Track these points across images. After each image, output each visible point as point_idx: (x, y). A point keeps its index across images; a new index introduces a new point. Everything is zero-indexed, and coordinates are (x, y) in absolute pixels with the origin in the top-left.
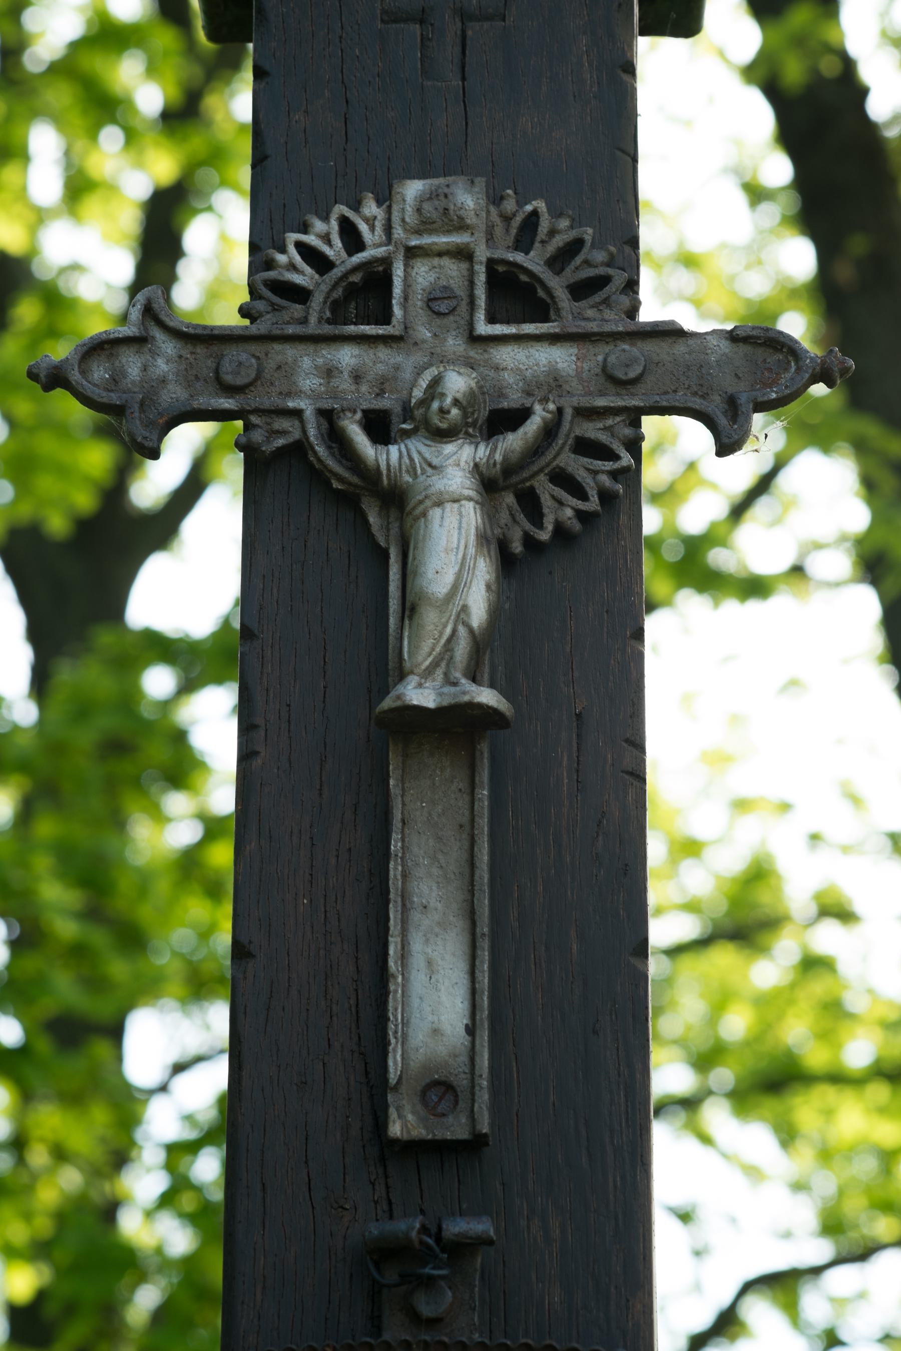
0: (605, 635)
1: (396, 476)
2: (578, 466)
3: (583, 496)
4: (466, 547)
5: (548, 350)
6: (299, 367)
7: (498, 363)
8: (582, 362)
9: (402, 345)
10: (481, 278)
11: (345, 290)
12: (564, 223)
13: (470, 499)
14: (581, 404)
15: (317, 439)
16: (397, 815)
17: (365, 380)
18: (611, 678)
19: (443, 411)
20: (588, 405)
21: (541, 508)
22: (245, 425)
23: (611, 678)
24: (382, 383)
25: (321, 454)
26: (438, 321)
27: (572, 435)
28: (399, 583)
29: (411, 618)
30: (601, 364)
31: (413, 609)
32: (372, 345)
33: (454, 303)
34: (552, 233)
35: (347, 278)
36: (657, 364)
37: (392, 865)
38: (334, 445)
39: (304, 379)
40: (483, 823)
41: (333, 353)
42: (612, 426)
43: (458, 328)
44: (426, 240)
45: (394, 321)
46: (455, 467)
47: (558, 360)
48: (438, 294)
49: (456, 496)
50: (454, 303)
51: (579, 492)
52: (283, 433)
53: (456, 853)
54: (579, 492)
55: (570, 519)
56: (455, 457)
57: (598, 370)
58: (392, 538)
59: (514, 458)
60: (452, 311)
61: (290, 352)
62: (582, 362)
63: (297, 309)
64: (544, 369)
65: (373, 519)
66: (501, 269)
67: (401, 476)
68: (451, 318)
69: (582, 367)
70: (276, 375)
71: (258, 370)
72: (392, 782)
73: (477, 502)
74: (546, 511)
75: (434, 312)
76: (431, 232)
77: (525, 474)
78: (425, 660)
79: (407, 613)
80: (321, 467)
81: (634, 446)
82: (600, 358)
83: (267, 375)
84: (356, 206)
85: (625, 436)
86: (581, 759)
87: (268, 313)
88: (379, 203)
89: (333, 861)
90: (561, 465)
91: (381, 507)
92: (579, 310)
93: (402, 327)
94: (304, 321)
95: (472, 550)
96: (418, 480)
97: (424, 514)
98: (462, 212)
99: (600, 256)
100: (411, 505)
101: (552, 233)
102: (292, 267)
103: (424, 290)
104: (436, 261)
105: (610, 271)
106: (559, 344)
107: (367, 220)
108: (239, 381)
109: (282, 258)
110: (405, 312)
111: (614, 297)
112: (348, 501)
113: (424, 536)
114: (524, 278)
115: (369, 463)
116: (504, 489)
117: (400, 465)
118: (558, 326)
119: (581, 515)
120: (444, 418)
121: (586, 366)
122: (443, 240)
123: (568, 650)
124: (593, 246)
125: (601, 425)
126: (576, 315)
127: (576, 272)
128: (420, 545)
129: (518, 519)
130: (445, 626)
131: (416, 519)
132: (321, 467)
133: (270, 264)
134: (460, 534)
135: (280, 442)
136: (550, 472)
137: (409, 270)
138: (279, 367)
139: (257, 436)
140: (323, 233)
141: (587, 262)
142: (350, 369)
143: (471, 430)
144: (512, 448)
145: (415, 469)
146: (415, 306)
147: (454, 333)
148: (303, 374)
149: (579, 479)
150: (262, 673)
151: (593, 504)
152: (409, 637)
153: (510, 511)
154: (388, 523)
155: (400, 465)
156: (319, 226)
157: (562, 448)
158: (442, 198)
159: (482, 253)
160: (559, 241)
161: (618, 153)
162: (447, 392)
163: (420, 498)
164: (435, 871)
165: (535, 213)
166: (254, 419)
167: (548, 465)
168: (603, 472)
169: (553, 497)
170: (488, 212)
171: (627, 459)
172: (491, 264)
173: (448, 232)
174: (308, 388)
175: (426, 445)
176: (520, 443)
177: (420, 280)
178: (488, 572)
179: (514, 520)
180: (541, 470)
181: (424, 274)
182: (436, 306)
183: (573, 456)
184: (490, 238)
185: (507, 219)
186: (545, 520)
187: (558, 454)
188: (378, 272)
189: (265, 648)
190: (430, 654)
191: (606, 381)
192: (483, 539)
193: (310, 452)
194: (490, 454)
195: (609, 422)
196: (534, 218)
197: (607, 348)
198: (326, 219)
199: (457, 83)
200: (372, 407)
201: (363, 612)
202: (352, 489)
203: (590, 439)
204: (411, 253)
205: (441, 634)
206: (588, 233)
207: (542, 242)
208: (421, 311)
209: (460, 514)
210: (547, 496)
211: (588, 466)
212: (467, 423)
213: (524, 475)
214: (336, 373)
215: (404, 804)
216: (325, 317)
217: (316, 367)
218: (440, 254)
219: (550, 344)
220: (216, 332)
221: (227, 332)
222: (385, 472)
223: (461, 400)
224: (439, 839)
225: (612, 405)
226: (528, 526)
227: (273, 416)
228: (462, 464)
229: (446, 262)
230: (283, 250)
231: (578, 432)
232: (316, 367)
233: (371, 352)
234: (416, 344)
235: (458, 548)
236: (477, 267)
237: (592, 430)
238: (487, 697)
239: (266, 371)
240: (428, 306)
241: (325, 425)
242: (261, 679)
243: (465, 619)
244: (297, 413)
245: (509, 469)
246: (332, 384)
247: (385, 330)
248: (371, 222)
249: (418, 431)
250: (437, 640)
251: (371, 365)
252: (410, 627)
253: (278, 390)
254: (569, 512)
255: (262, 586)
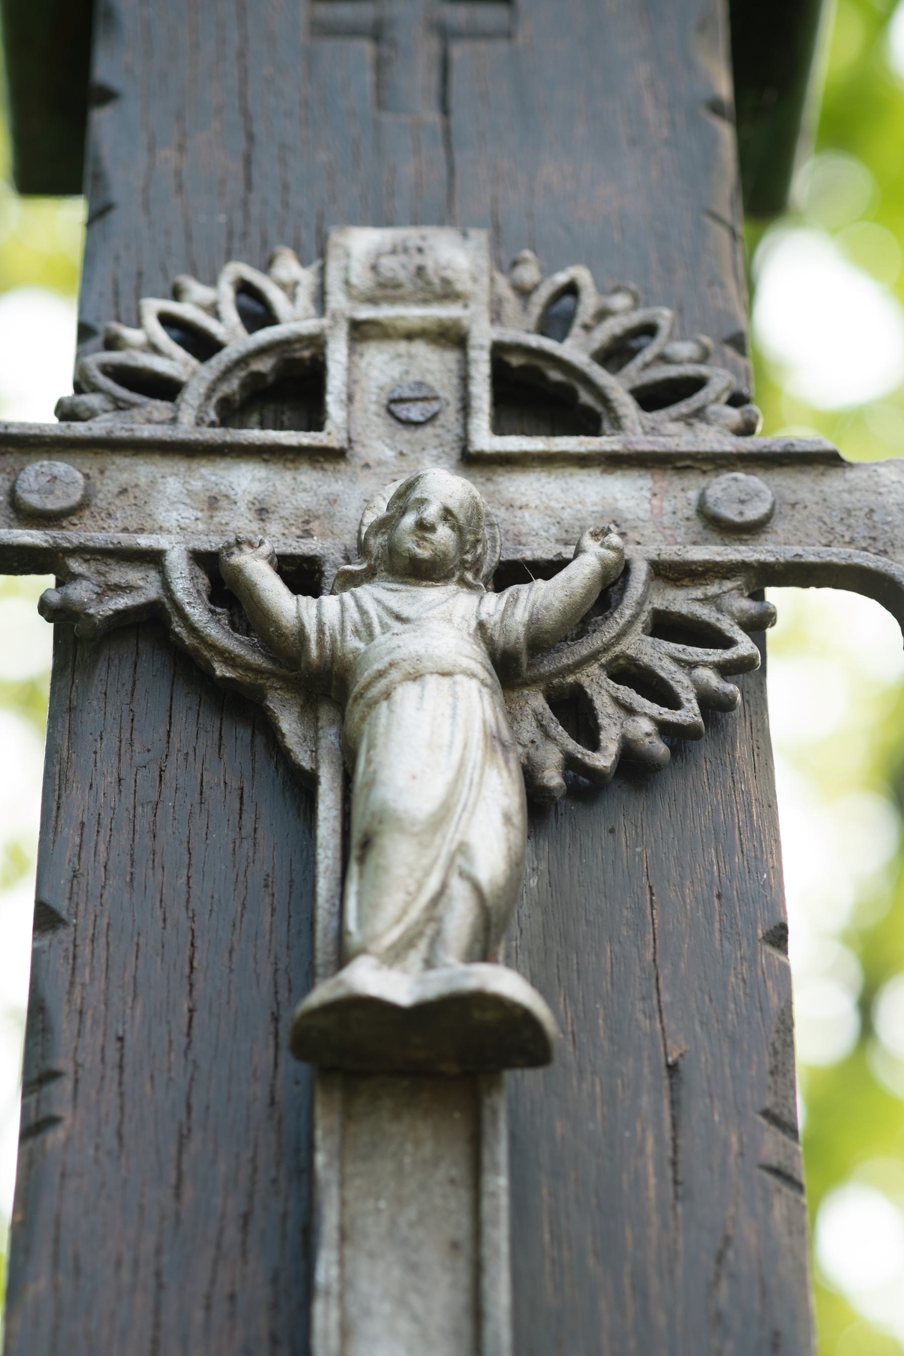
0: (717, 935)
1: (334, 641)
2: (659, 655)
3: (671, 700)
4: (465, 746)
5: (600, 481)
6: (159, 492)
7: (512, 499)
8: (662, 500)
9: (342, 466)
10: (481, 371)
11: (243, 385)
12: (620, 302)
13: (473, 675)
14: (664, 557)
15: (190, 594)
16: (330, 1219)
17: (276, 516)
18: (732, 1006)
19: (423, 527)
20: (676, 558)
21: (595, 717)
22: (57, 580)
23: (732, 1006)
24: (307, 522)
25: (196, 618)
26: (406, 434)
27: (648, 607)
28: (337, 825)
29: (362, 860)
30: (694, 503)
31: (367, 844)
32: (289, 465)
33: (434, 406)
34: (603, 314)
35: (247, 364)
36: (793, 505)
37: (318, 1308)
38: (219, 610)
39: (167, 511)
40: (499, 1235)
41: (221, 473)
42: (718, 596)
43: (441, 445)
44: (384, 313)
45: (329, 426)
46: (445, 624)
47: (619, 496)
48: (407, 394)
49: (447, 667)
50: (434, 406)
51: (663, 694)
52: (128, 589)
53: (443, 1295)
54: (663, 694)
55: (648, 735)
56: (443, 607)
57: (691, 512)
58: (323, 753)
59: (550, 619)
60: (432, 418)
61: (143, 470)
62: (662, 500)
63: (159, 408)
64: (595, 509)
65: (289, 724)
66: (515, 361)
67: (343, 640)
68: (429, 430)
69: (661, 508)
70: (117, 502)
71: (86, 489)
72: (320, 1159)
73: (483, 683)
74: (603, 721)
75: (399, 420)
76: (393, 300)
77: (567, 660)
78: (389, 928)
79: (355, 852)
80: (195, 642)
81: (758, 625)
82: (693, 495)
83: (100, 501)
84: (267, 265)
85: (742, 611)
86: (681, 1142)
87: (106, 411)
88: (304, 262)
89: (199, 1315)
90: (629, 652)
91: (302, 707)
92: (652, 424)
93: (344, 435)
94: (174, 420)
95: (476, 753)
96: (376, 642)
97: (387, 695)
98: (449, 274)
99: (684, 349)
100: (363, 680)
101: (603, 314)
102: (153, 348)
103: (381, 388)
104: (402, 346)
105: (703, 370)
106: (619, 473)
107: (283, 286)
108: (52, 504)
109: (133, 335)
110: (349, 414)
111: (712, 408)
112: (238, 706)
113: (388, 727)
114: (555, 375)
115: (284, 623)
116: (532, 682)
117: (343, 622)
118: (619, 441)
119: (665, 729)
120: (424, 539)
121: (668, 506)
122: (414, 314)
123: (649, 956)
124: (671, 337)
125: (698, 593)
126: (647, 429)
127: (640, 371)
128: (380, 741)
129: (553, 732)
130: (427, 873)
131: (373, 704)
132: (195, 642)
133: (112, 343)
134: (454, 724)
135: (122, 602)
136: (610, 662)
137: (356, 358)
138: (123, 491)
139: (80, 592)
140: (209, 302)
141: (663, 359)
142: (250, 498)
143: (469, 576)
144: (545, 603)
145: (369, 626)
146: (366, 411)
147: (435, 452)
148: (166, 503)
149: (663, 674)
150: (72, 984)
151: (689, 713)
152: (360, 894)
153: (537, 720)
154: (317, 730)
155: (343, 622)
156: (198, 291)
157: (630, 623)
158: (413, 251)
159: (483, 335)
160: (613, 327)
161: (708, 221)
162: (431, 497)
163: (378, 666)
164: (404, 1325)
165: (571, 289)
166: (76, 565)
167: (606, 648)
168: (705, 664)
169: (616, 701)
170: (492, 280)
171: (745, 646)
172: (499, 350)
173: (425, 302)
174: (175, 524)
175: (392, 590)
176: (561, 594)
177: (374, 373)
178: (506, 794)
179: (547, 735)
180: (593, 657)
181: (382, 366)
182: (403, 411)
183: (650, 639)
184: (496, 317)
185: (524, 293)
186: (603, 736)
187: (623, 634)
188: (300, 361)
189: (78, 942)
190: (398, 920)
191: (705, 528)
192: (494, 740)
193: (175, 619)
194: (505, 610)
195: (713, 589)
196: (567, 301)
197: (703, 481)
198: (212, 282)
199: (433, 116)
200: (289, 550)
201: (266, 886)
202: (249, 678)
203: (680, 615)
204: (360, 332)
205: (420, 886)
206: (664, 316)
207: (587, 328)
208: (375, 419)
209: (454, 696)
210: (606, 699)
211: (677, 655)
212: (463, 562)
213: (565, 661)
214: (224, 503)
215: (343, 1203)
216: (207, 420)
217: (190, 493)
218: (410, 336)
219: (604, 471)
220: (13, 431)
221: (32, 432)
222: (313, 636)
223: (456, 511)
224: (412, 1267)
225: (718, 559)
226: (572, 746)
227: (110, 561)
228: (457, 620)
229: (420, 348)
230: (138, 324)
231: (658, 602)
232: (190, 493)
233: (288, 476)
234: (367, 466)
235: (451, 746)
236: (473, 354)
237: (682, 601)
238: (507, 983)
239: (101, 496)
240: (390, 412)
241: (203, 581)
242: (70, 993)
243: (465, 866)
244: (153, 559)
245: (540, 642)
246: (216, 519)
247: (314, 438)
248: (290, 289)
249: (374, 575)
250: (413, 896)
251: (287, 493)
252: (361, 875)
253: (120, 525)
254: (645, 726)
255: (77, 840)
